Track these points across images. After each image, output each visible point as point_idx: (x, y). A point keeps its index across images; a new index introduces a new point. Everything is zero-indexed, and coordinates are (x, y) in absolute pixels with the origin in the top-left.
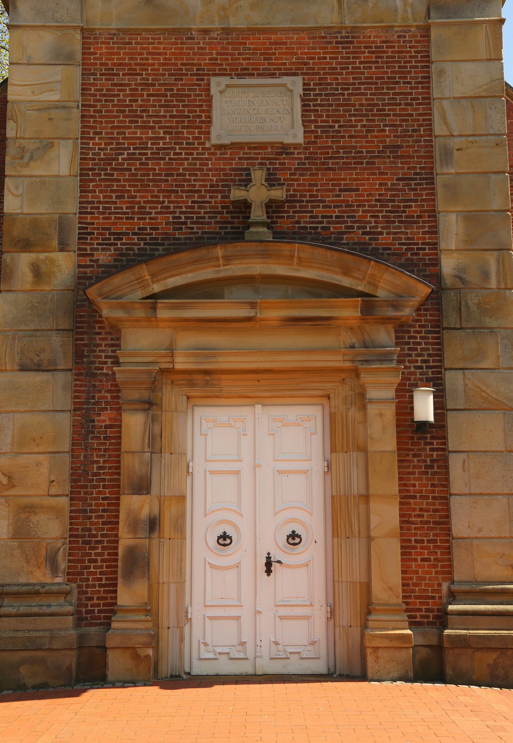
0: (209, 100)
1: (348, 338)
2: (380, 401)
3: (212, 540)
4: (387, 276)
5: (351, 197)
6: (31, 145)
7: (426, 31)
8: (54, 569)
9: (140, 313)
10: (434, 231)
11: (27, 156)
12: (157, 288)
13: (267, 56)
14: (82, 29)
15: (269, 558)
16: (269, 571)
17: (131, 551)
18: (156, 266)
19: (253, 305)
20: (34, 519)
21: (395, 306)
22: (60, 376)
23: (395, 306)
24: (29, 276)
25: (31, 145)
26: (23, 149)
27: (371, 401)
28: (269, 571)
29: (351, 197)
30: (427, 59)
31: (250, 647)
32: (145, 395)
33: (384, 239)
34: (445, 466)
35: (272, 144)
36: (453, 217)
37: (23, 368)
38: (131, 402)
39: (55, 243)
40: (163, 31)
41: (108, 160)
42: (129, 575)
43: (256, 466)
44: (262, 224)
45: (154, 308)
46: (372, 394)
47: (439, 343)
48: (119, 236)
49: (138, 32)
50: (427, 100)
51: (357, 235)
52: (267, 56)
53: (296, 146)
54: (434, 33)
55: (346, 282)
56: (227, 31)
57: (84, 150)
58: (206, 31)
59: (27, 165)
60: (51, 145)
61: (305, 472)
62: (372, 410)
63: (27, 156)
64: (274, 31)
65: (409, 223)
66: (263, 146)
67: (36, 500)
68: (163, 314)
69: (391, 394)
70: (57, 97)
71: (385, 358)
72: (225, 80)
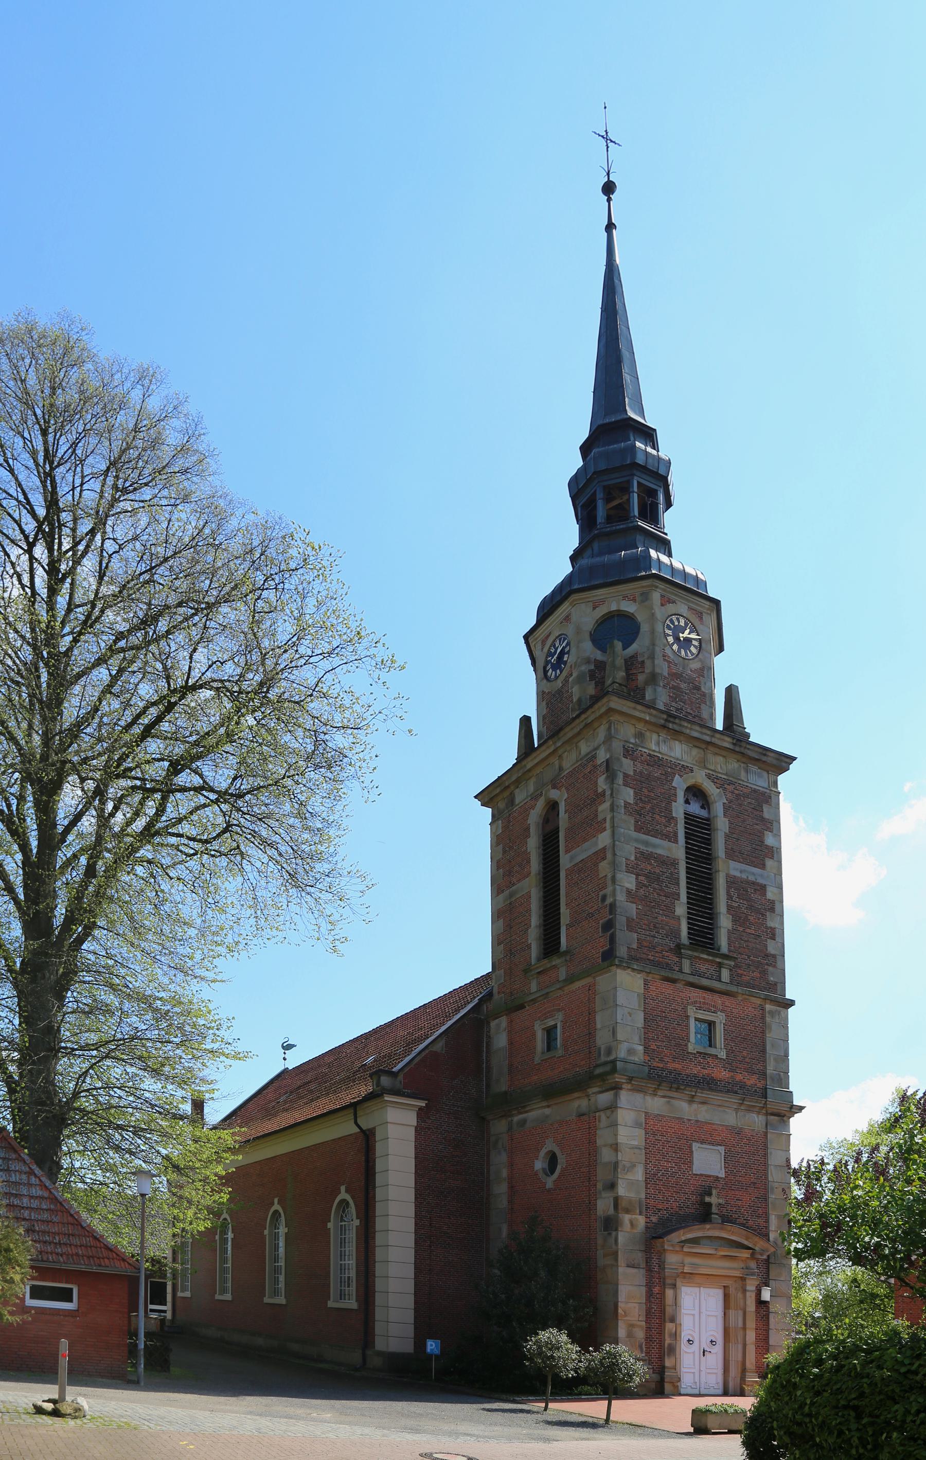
0: (692, 1152)
1: (742, 1265)
2: (751, 1291)
3: (708, 1342)
4: (761, 1243)
5: (739, 1203)
6: (628, 1165)
7: (766, 1134)
8: (642, 1352)
9: (678, 1249)
10: (767, 1221)
11: (626, 1170)
12: (683, 1238)
13: (711, 1135)
14: (646, 1112)
15: (704, 1350)
16: (704, 1355)
17: (670, 1345)
18: (686, 1230)
19: (716, 1249)
20: (635, 1330)
21: (762, 1255)
22: (641, 1270)
23: (762, 1255)
24: (629, 1225)
25: (628, 1165)
26: (624, 1166)
27: (748, 1291)
28: (704, 1355)
29: (739, 1203)
30: (766, 1147)
31: (698, 1384)
32: (673, 1282)
33: (751, 1223)
34: (768, 1318)
35: (713, 1176)
36: (774, 1216)
37: (628, 1266)
38: (670, 1285)
39: (638, 1211)
40: (674, 1118)
41: (655, 1175)
42: (669, 1355)
43: (700, 1313)
44: (717, 1214)
45: (683, 1247)
46: (748, 1288)
47: (768, 1269)
48: (659, 1210)
49: (664, 1116)
50: (766, 1165)
51: (742, 1220)
52: (711, 1135)
53: (721, 1178)
54: (769, 1136)
55: (746, 1243)
56: (697, 1121)
57: (646, 1169)
58: (689, 1120)
59: (626, 1173)
60: (635, 1166)
61: (716, 1316)
62: (748, 1294)
63: (626, 1170)
64: (713, 1124)
65: (758, 1217)
66: (710, 1176)
67: (635, 1322)
68: (685, 1250)
69: (754, 1288)
70: (636, 1143)
71: (753, 1274)
72: (699, 1145)
